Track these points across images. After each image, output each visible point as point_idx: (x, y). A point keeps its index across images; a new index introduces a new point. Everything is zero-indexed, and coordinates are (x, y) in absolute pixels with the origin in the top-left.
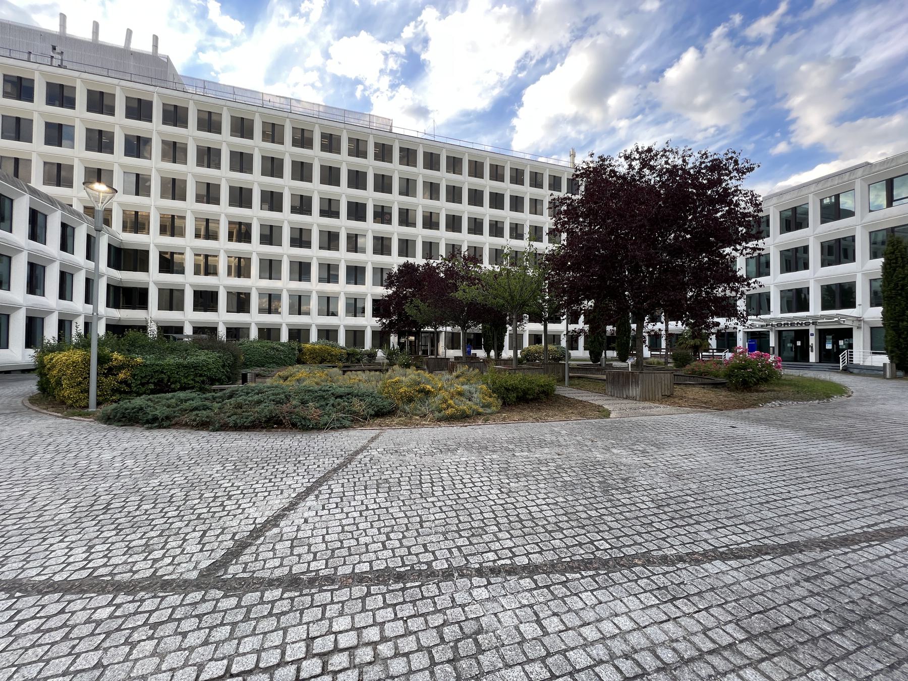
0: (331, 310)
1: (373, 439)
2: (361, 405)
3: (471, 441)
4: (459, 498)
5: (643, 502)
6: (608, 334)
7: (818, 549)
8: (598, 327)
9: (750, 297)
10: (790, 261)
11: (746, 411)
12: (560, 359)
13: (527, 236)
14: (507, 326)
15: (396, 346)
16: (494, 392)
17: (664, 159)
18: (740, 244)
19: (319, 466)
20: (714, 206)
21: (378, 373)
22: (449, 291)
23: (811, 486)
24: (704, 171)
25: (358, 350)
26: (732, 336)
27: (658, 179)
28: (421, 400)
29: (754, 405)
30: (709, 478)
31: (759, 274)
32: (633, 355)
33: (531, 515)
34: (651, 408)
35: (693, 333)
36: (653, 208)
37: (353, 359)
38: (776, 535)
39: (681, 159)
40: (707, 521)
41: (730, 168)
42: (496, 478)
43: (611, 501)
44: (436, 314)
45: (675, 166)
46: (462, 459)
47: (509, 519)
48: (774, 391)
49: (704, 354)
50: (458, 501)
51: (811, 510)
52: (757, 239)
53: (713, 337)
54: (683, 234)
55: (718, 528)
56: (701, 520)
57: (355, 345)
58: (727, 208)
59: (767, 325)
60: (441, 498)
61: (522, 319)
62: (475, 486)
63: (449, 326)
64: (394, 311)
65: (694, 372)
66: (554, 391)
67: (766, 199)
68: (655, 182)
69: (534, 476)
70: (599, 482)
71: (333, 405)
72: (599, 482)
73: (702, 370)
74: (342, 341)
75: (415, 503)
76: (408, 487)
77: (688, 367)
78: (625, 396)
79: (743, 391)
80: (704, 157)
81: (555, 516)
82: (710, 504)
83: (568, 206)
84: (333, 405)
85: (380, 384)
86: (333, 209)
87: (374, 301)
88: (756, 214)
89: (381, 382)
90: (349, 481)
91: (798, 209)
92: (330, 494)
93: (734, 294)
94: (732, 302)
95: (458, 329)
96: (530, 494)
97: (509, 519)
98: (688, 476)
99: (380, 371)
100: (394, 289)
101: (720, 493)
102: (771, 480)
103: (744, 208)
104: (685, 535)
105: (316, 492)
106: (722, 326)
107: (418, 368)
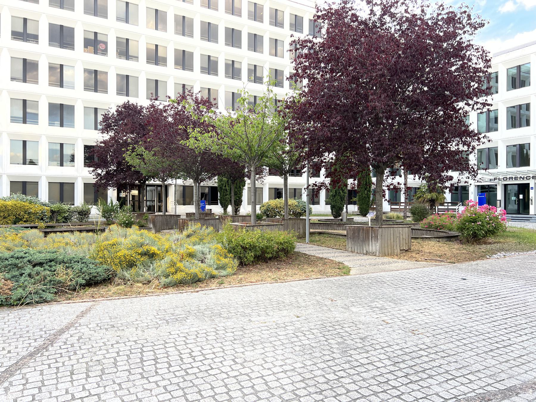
0: (29, 157)
1: (83, 314)
2: (67, 274)
3: (203, 308)
4: (187, 374)
5: (380, 360)
6: (349, 188)
7: (531, 390)
8: (338, 181)
9: (481, 151)
10: (515, 117)
11: (475, 263)
12: (301, 214)
13: (266, 79)
14: (246, 179)
15: (115, 202)
16: (230, 252)
17: (404, 7)
18: (472, 99)
19: (9, 352)
20: (449, 60)
21: (91, 234)
22: (179, 138)
23: (527, 332)
24: (440, 23)
25: (66, 207)
26: (465, 189)
27: (398, 27)
28: (145, 265)
29: (482, 257)
30: (441, 331)
31: (489, 130)
32: (373, 209)
33: (267, 385)
34: (390, 263)
35: (429, 187)
36: (393, 57)
37: (59, 218)
38: (498, 382)
39: (420, 9)
40: (439, 374)
41: (464, 22)
42: (230, 347)
43: (349, 362)
44: (164, 164)
45: (414, 16)
46: (192, 329)
47: (242, 392)
48: (500, 242)
49: (440, 207)
50: (186, 377)
51: (527, 354)
52: (487, 94)
53: (447, 191)
54: (420, 86)
55: (448, 380)
56: (434, 373)
57: (62, 200)
58: (461, 62)
59: (495, 179)
60: (166, 376)
61: (262, 172)
62: (206, 359)
63: (179, 178)
64: (112, 160)
65: (430, 226)
66: (294, 248)
67: (497, 55)
68: (395, 30)
69: (271, 342)
70: (338, 343)
71: (30, 275)
72: (338, 343)
73: (437, 224)
74: (44, 195)
75: (135, 385)
76: (127, 367)
77: (425, 221)
78: (365, 252)
79: (473, 244)
80: (441, 8)
81: (292, 384)
82: (442, 357)
83: (310, 49)
84: (30, 275)
85: (93, 247)
86: (30, 31)
87: (87, 148)
88: (485, 69)
89: (94, 246)
90: (50, 367)
91: (522, 67)
92: (24, 385)
93: (466, 148)
94: (465, 156)
95: (190, 182)
96: (266, 362)
97: (242, 392)
98: (423, 331)
99: (92, 231)
100: (112, 134)
101: (451, 346)
102: (495, 329)
103: (476, 63)
104: (419, 390)
105: (6, 384)
106: (455, 180)
107: (142, 227)
